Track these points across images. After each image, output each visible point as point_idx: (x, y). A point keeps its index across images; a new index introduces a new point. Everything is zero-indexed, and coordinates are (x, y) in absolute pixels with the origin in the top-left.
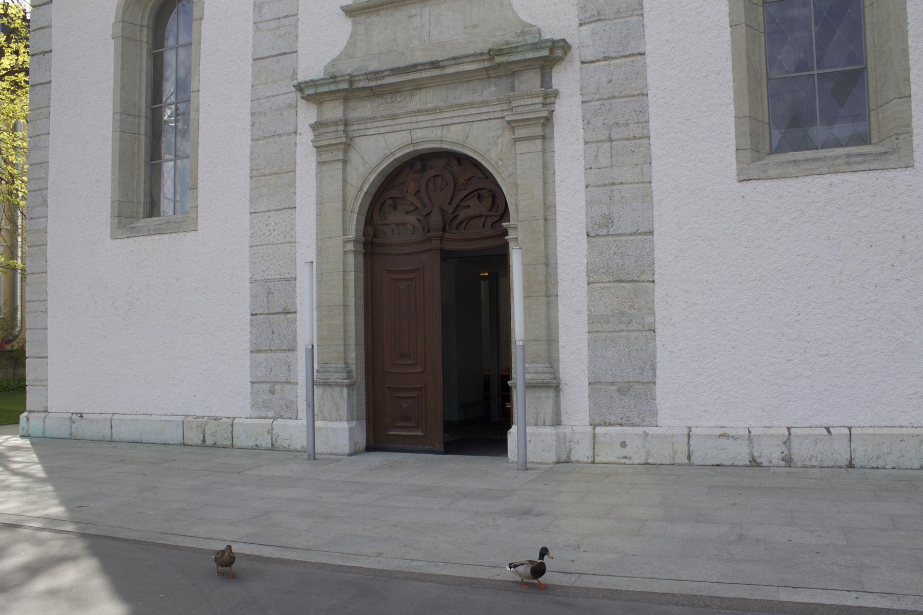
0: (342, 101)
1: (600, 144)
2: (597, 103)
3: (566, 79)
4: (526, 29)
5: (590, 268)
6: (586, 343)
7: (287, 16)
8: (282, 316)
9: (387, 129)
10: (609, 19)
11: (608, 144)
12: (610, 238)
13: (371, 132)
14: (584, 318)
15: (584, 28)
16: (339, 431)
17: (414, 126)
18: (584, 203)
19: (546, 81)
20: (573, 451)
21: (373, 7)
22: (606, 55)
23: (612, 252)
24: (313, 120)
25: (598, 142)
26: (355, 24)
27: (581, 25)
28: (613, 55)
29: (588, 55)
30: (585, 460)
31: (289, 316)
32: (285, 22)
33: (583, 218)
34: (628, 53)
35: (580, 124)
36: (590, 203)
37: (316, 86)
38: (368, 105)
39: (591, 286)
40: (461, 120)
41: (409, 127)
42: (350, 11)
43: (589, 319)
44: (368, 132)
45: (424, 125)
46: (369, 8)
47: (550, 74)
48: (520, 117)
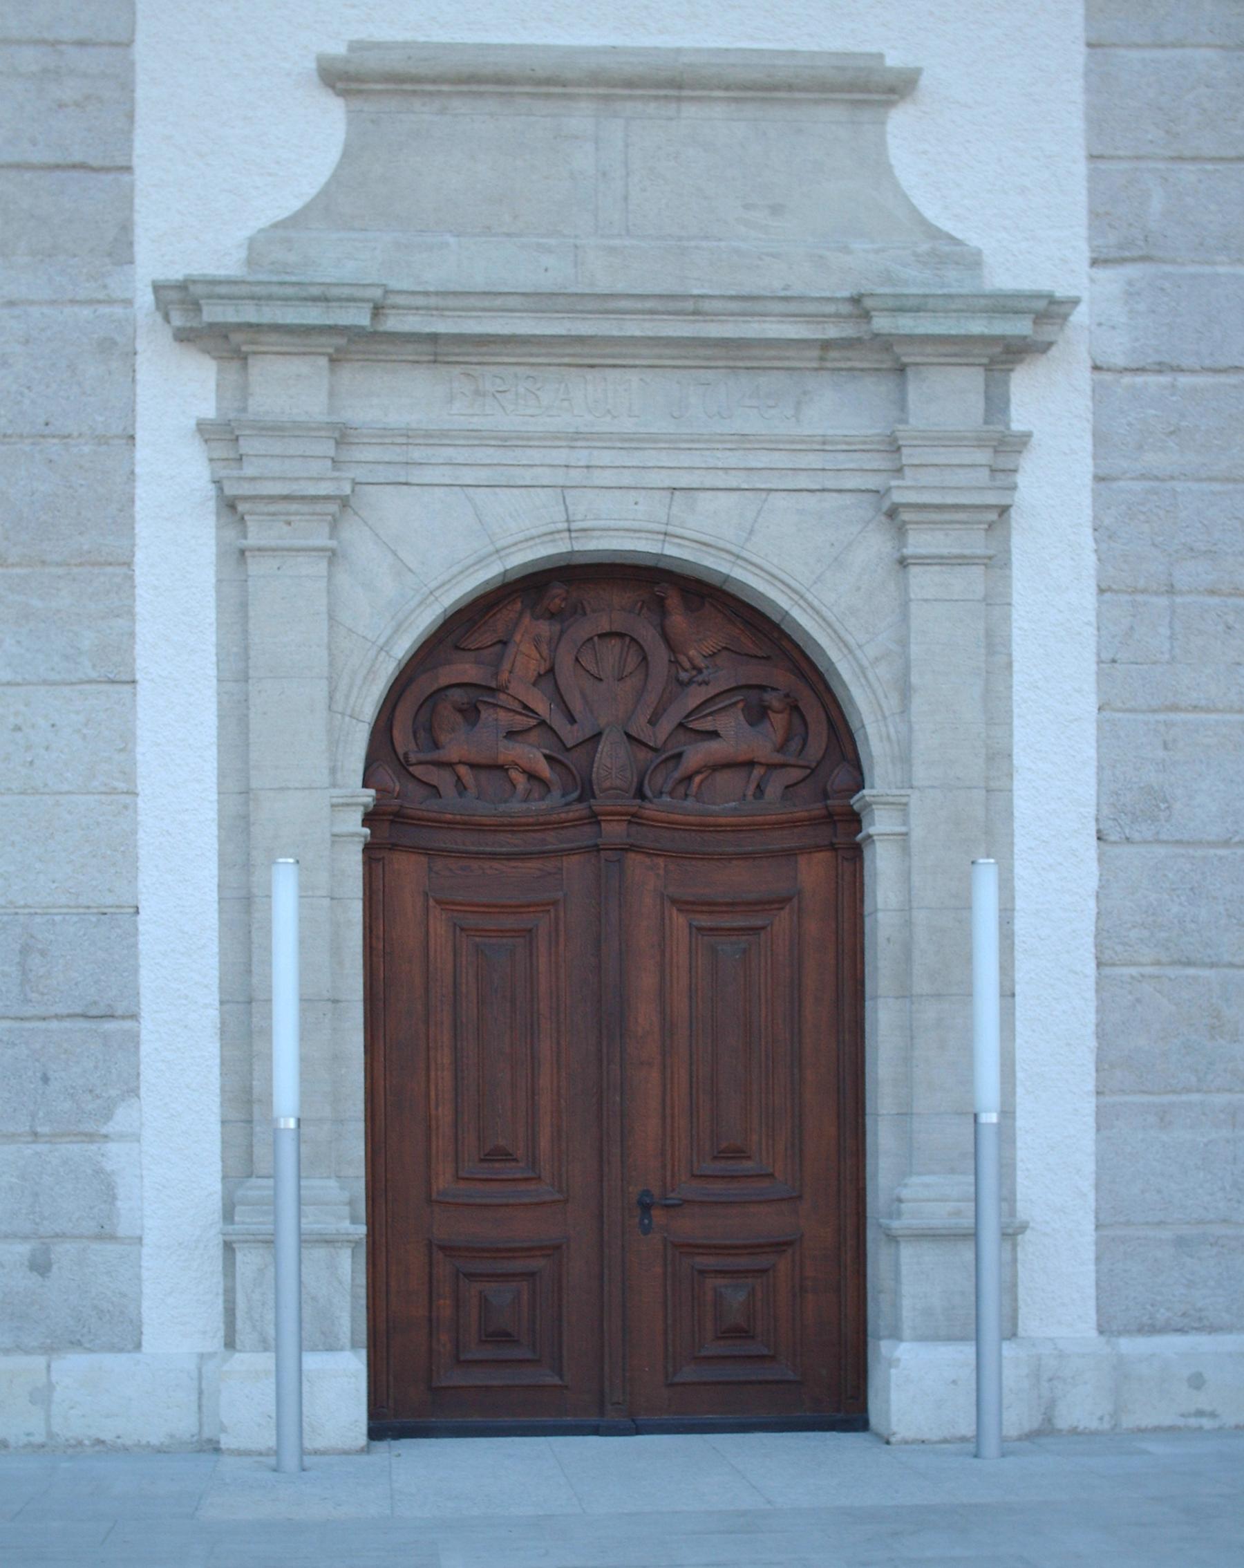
0: (323, 362)
2: (1138, 486)
3: (1052, 407)
11: (1163, 601)
12: (1161, 851)
13: (428, 475)
15: (1102, 274)
16: (340, 1383)
17: (576, 476)
19: (997, 404)
22: (1166, 359)
24: (208, 409)
25: (1135, 591)
28: (1186, 362)
30: (1094, 1425)
31: (109, 1026)
34: (1224, 362)
39: (1107, 971)
41: (560, 477)
42: (341, 79)
44: (416, 476)
45: (608, 478)
47: (1006, 383)
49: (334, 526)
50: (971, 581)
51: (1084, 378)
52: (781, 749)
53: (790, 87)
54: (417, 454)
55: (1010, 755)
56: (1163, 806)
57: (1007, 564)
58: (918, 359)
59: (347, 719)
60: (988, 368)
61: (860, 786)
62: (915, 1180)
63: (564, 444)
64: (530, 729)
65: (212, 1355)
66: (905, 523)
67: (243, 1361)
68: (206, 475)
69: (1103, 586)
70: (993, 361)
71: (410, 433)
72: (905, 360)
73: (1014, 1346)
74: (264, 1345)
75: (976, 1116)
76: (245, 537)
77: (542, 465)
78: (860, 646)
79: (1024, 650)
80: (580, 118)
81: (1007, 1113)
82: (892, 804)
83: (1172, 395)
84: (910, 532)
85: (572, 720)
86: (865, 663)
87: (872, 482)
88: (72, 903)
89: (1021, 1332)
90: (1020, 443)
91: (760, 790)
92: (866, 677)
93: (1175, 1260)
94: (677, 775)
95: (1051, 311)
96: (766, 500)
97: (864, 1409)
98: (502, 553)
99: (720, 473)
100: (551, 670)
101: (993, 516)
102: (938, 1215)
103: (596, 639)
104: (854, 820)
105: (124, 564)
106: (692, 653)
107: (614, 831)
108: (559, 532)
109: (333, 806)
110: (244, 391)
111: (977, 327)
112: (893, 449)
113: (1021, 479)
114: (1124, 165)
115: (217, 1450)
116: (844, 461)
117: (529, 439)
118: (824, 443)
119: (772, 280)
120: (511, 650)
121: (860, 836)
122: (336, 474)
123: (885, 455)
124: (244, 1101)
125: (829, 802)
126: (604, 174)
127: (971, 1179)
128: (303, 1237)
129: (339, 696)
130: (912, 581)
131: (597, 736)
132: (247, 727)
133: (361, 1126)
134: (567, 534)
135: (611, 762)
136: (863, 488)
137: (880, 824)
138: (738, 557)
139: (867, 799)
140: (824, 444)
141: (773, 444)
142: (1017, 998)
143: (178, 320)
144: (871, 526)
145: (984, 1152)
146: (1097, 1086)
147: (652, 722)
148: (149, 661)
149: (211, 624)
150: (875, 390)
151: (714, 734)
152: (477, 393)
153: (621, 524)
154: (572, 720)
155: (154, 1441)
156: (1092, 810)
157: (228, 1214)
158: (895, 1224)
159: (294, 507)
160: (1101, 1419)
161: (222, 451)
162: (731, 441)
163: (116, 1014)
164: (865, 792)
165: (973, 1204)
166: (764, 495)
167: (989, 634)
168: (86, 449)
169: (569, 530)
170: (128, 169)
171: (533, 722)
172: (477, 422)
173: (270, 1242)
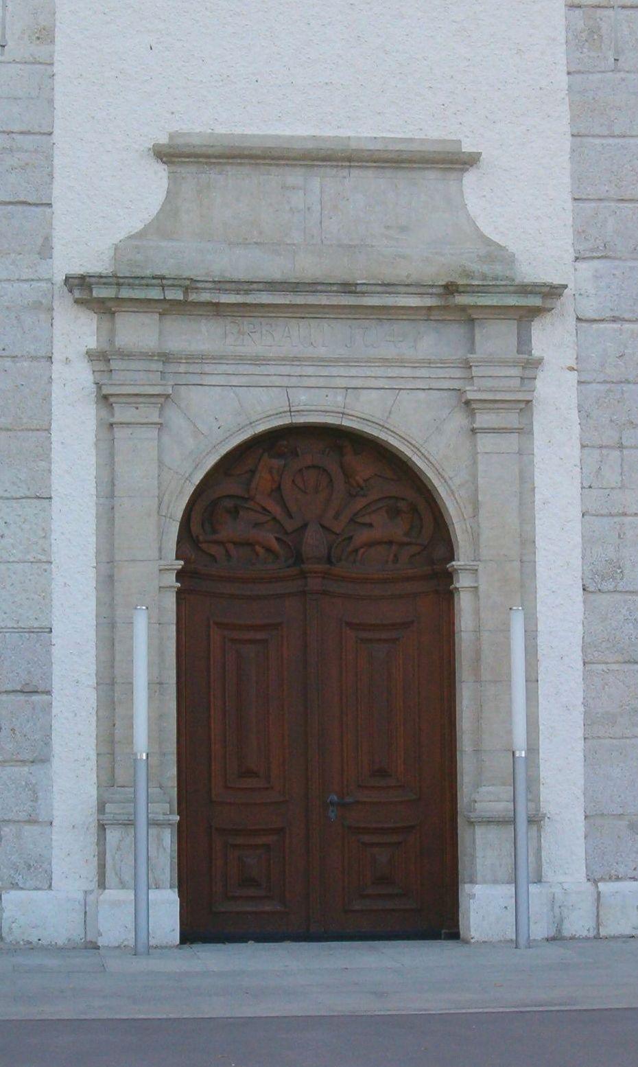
1: (605, 452)
3: (552, 340)
4: (495, 253)
5: (588, 640)
6: (581, 755)
7: (28, 133)
8: (22, 698)
9: (244, 380)
10: (620, 259)
11: (617, 453)
12: (618, 597)
14: (578, 715)
15: (582, 265)
16: (166, 909)
18: (578, 539)
19: (524, 342)
20: (566, 922)
21: (220, 157)
22: (617, 314)
23: (621, 617)
24: (92, 343)
26: (174, 179)
27: (577, 259)
29: (589, 308)
30: (585, 933)
31: (35, 698)
32: (27, 142)
33: (577, 562)
35: (574, 416)
36: (588, 541)
37: (118, 284)
38: (204, 329)
39: (588, 667)
40: (381, 383)
42: (171, 155)
43: (585, 719)
46: (208, 157)
48: (490, 396)
49: (162, 409)
50: (510, 443)
51: (572, 321)
52: (407, 534)
53: (411, 161)
54: (207, 369)
55: (534, 542)
56: (619, 571)
57: (531, 432)
58: (481, 316)
59: (168, 519)
60: (520, 320)
61: (452, 558)
62: (483, 789)
63: (288, 363)
64: (266, 522)
65: (92, 891)
66: (474, 409)
67: (111, 894)
68: (91, 378)
69: (584, 444)
70: (521, 317)
71: (203, 357)
72: (475, 316)
73: (539, 886)
74: (123, 885)
75: (513, 753)
76: (113, 415)
77: (275, 375)
78: (451, 478)
79: (541, 480)
80: (295, 177)
81: (533, 750)
82: (469, 570)
83: (620, 335)
84: (477, 414)
85: (290, 516)
86: (453, 488)
87: (456, 385)
88: (15, 626)
89: (544, 879)
90: (537, 363)
91: (396, 559)
92: (454, 496)
93: (637, 832)
94: (349, 549)
95: (553, 292)
96: (398, 394)
97: (456, 924)
98: (253, 424)
99: (373, 379)
100: (279, 488)
101: (522, 405)
102: (500, 807)
103: (304, 469)
104: (449, 576)
105: (46, 430)
106: (358, 478)
107: (314, 583)
108: (285, 412)
109: (160, 570)
110: (112, 332)
111: (512, 301)
112: (468, 366)
113: (538, 383)
114: (593, 205)
115: (98, 948)
116: (441, 373)
117: (269, 360)
118: (430, 363)
119: (401, 272)
120: (257, 476)
121: (452, 587)
122: (163, 382)
123: (462, 369)
124: (112, 742)
125: (435, 567)
126: (309, 209)
127: (512, 788)
128: (149, 822)
129: (164, 506)
130: (479, 442)
131: (305, 526)
132: (113, 524)
133: (174, 758)
134: (289, 414)
135: (313, 541)
136: (452, 388)
137: (463, 581)
138: (383, 426)
139: (455, 567)
140: (428, 363)
141: (401, 362)
142: (539, 682)
143: (77, 294)
144: (456, 410)
145: (524, 774)
146: (584, 735)
147: (336, 517)
148: (59, 486)
149: (93, 465)
150: (455, 333)
151: (371, 525)
152: (239, 332)
153: (319, 408)
154: (290, 516)
155: (60, 943)
156: (579, 574)
157: (101, 808)
158: (472, 815)
159: (141, 400)
160: (588, 930)
161: (101, 366)
162: (379, 362)
163: (39, 690)
164: (454, 563)
165: (512, 803)
166: (397, 391)
167: (521, 472)
168: (26, 364)
169: (290, 412)
170: (50, 205)
171: (269, 518)
172: (242, 350)
173: (130, 823)
